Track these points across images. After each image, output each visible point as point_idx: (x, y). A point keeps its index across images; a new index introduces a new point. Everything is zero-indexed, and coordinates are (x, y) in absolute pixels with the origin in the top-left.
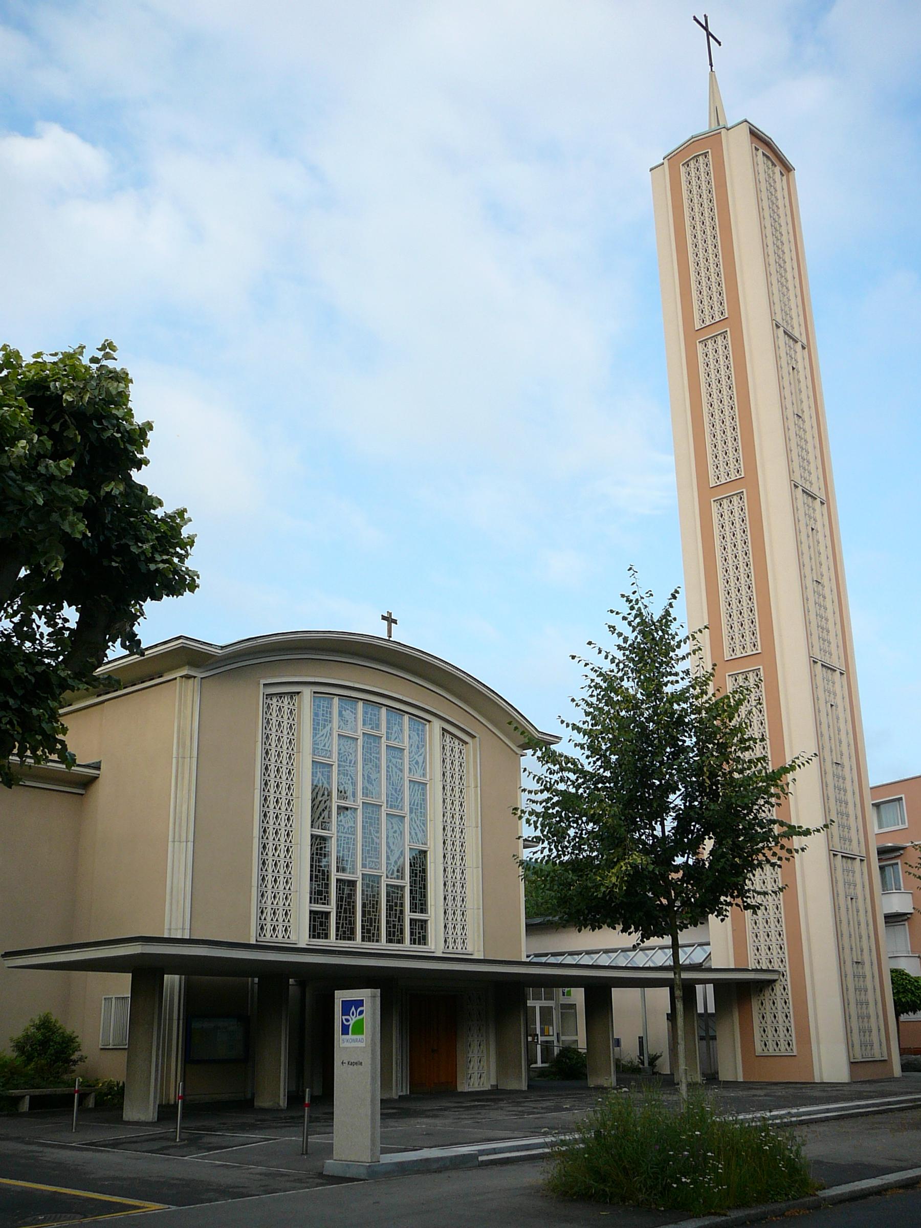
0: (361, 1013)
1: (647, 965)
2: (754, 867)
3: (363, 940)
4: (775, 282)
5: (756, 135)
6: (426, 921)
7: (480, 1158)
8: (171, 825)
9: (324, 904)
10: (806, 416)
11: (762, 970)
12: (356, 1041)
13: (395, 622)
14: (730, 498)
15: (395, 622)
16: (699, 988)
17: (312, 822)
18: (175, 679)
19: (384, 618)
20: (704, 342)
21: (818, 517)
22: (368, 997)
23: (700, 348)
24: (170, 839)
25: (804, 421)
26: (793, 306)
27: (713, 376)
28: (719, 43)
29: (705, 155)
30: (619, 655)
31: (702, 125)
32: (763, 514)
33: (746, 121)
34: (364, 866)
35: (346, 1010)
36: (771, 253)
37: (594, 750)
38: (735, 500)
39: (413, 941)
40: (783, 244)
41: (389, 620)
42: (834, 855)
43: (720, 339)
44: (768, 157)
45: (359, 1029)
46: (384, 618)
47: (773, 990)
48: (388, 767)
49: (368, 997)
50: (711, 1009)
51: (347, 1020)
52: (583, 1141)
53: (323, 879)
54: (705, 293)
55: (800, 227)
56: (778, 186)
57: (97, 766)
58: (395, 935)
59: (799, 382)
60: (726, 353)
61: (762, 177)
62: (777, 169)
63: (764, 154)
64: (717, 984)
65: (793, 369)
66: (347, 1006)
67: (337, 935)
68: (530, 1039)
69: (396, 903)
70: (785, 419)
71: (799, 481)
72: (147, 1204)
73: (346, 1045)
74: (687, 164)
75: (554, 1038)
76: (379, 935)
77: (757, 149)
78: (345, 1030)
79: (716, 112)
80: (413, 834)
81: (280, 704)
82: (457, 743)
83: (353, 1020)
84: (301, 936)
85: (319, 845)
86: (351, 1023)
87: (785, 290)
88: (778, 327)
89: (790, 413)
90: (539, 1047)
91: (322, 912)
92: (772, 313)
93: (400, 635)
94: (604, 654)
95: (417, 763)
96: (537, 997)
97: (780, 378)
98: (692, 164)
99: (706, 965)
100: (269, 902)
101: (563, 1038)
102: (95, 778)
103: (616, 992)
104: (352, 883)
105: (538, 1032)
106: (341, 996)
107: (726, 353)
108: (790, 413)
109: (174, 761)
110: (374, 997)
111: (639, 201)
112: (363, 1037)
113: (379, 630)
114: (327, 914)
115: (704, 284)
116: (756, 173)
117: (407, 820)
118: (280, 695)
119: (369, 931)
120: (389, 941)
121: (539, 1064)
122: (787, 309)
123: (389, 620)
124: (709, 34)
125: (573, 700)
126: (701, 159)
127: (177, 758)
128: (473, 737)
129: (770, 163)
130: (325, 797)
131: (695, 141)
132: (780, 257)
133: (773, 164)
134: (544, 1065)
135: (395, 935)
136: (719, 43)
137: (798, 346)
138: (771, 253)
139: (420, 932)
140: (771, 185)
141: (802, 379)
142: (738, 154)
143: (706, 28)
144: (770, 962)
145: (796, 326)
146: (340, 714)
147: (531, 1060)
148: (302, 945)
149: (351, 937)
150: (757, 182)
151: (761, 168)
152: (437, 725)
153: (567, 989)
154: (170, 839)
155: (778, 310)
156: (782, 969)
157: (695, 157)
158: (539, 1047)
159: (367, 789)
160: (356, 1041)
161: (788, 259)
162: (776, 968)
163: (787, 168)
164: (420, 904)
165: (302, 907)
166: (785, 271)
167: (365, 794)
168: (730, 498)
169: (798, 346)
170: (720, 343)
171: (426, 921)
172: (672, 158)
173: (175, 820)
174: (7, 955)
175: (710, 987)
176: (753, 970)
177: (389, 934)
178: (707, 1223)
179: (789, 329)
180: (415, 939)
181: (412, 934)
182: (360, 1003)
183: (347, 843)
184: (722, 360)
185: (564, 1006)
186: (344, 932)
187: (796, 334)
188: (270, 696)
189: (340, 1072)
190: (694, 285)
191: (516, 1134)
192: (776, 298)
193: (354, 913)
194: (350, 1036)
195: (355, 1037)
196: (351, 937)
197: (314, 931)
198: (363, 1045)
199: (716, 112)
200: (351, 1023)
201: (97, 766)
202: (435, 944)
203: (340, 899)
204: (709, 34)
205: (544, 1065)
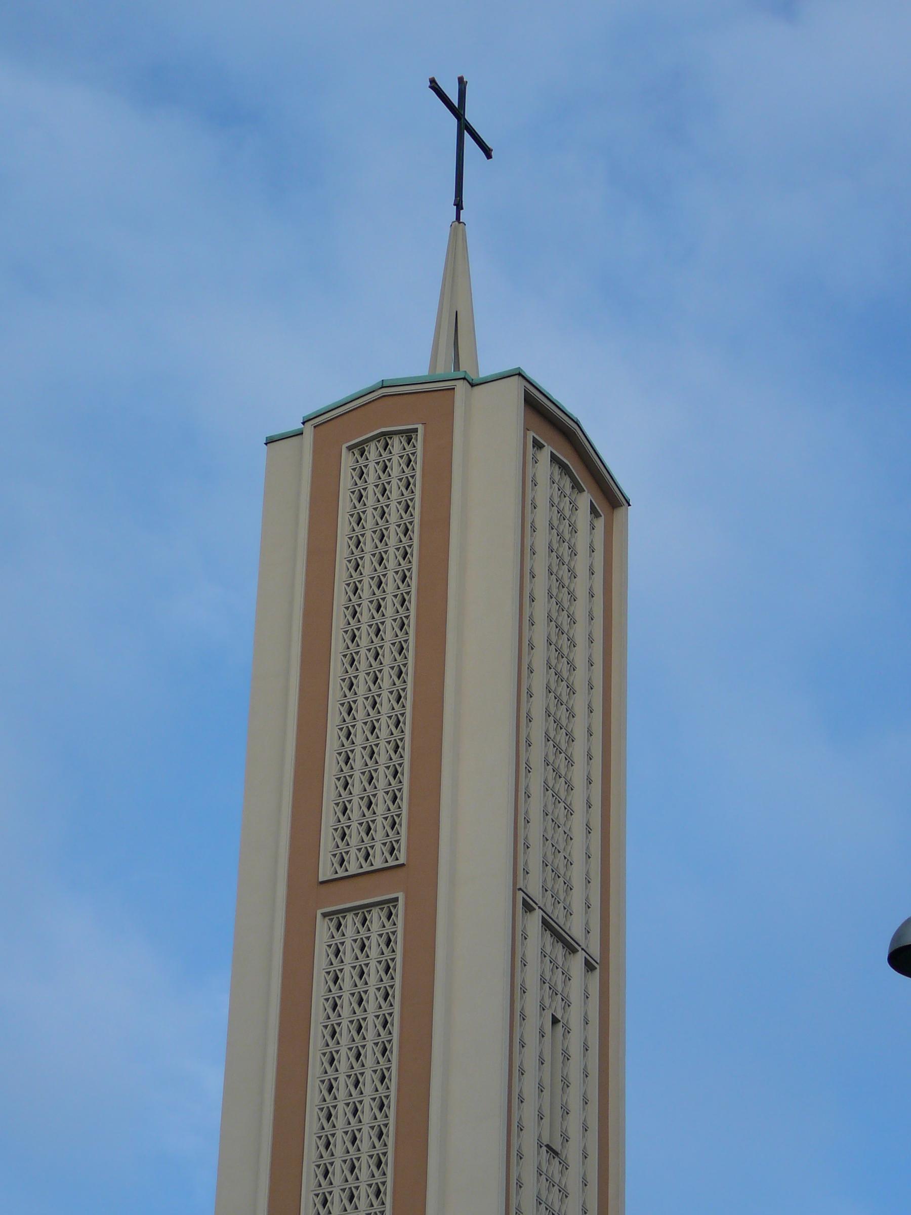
4: (536, 789)
5: (540, 410)
10: (572, 1153)
14: (362, 912)
20: (336, 917)
21: (575, 996)
23: (323, 930)
25: (565, 1166)
26: (578, 856)
27: (348, 958)
28: (488, 153)
29: (409, 435)
31: (410, 357)
32: (433, 1073)
33: (520, 374)
36: (538, 713)
40: (572, 691)
43: (376, 917)
44: (563, 467)
54: (356, 789)
55: (624, 613)
56: (581, 541)
59: (567, 1057)
60: (387, 982)
61: (542, 517)
62: (584, 500)
63: (554, 458)
65: (555, 1021)
70: (512, 1155)
71: (535, 890)
74: (360, 449)
77: (538, 445)
79: (455, 329)
87: (561, 811)
88: (528, 907)
89: (528, 1142)
92: (518, 870)
97: (515, 1043)
98: (373, 451)
107: (387, 982)
108: (528, 1142)
111: (223, 576)
115: (363, 666)
116: (526, 505)
122: (560, 862)
126: (396, 444)
129: (567, 483)
131: (388, 395)
132: (560, 630)
133: (577, 487)
136: (488, 153)
137: (577, 963)
138: (538, 713)
140: (562, 521)
141: (575, 1050)
142: (488, 447)
143: (458, 112)
145: (577, 905)
150: (526, 527)
151: (543, 493)
155: (535, 866)
157: (382, 436)
161: (579, 732)
163: (611, 498)
166: (570, 761)
168: (362, 912)
169: (577, 963)
170: (375, 926)
172: (325, 422)
179: (558, 914)
184: (382, 778)
187: (575, 929)
190: (338, 644)
192: (535, 832)
199: (455, 329)
204: (464, 127)
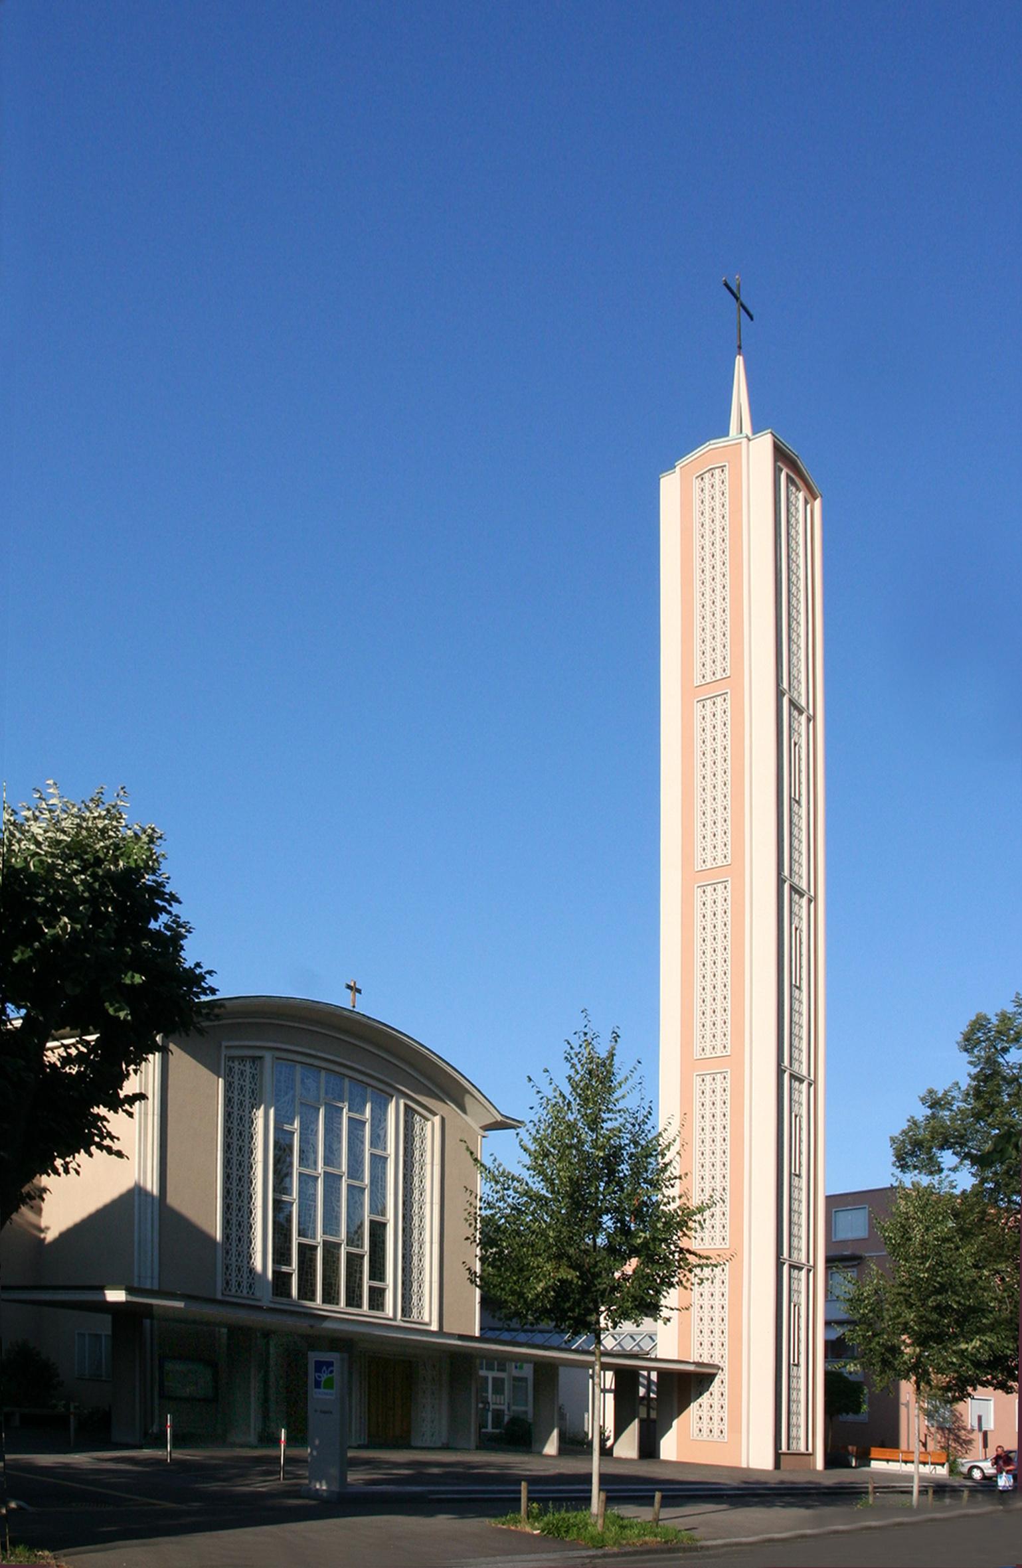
0: (332, 1372)
2: (671, 1285)
15: (359, 991)
29: (722, 468)
30: (533, 1147)
37: (540, 1171)
38: (720, 887)
45: (329, 1384)
46: (349, 987)
58: (354, 1299)
66: (319, 1366)
68: (481, 1406)
75: (505, 1407)
78: (318, 1384)
81: (242, 1067)
86: (323, 1379)
90: (490, 1414)
94: (553, 1086)
100: (234, 1259)
101: (514, 1408)
104: (314, 1248)
106: (314, 1356)
118: (242, 1059)
121: (490, 1429)
125: (467, 1238)
134: (497, 1431)
135: (354, 1299)
146: (302, 1082)
147: (483, 1425)
158: (490, 1414)
162: (716, 1363)
164: (378, 1272)
167: (326, 1164)
176: (694, 1363)
182: (330, 1364)
185: (515, 1379)
188: (231, 1059)
194: (322, 1390)
205: (497, 1431)
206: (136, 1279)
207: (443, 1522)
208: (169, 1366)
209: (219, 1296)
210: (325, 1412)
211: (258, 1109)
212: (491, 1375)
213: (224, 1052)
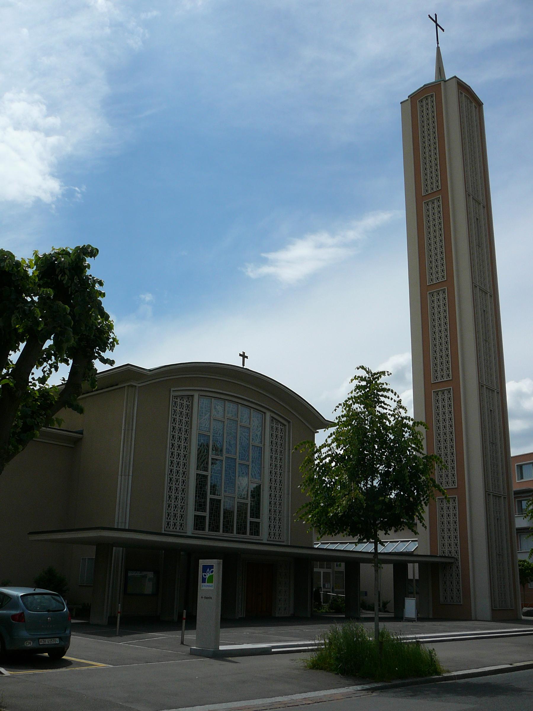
0: (212, 572)
1: (383, 552)
3: (223, 532)
6: (259, 523)
7: (273, 650)
8: (120, 466)
9: (202, 511)
11: (445, 557)
12: (209, 586)
13: (247, 357)
15: (247, 357)
16: (410, 566)
17: (197, 467)
18: (125, 387)
19: (240, 355)
22: (216, 563)
24: (120, 473)
28: (443, 30)
34: (225, 491)
35: (204, 571)
39: (251, 534)
41: (244, 356)
42: (489, 494)
45: (211, 580)
46: (240, 355)
47: (451, 568)
48: (240, 437)
49: (216, 563)
50: (417, 577)
51: (205, 575)
52: (325, 644)
53: (203, 498)
57: (81, 433)
64: (420, 563)
67: (209, 529)
69: (242, 512)
72: (99, 664)
73: (204, 588)
76: (233, 530)
78: (204, 581)
80: (253, 474)
81: (182, 402)
82: (279, 425)
83: (208, 575)
84: (190, 529)
85: (201, 481)
86: (207, 577)
91: (201, 516)
93: (249, 365)
95: (257, 435)
96: (322, 567)
99: (415, 553)
102: (80, 439)
103: (361, 565)
105: (322, 586)
106: (202, 562)
109: (123, 431)
110: (219, 564)
112: (213, 584)
113: (237, 362)
114: (204, 517)
117: (250, 467)
118: (182, 397)
119: (227, 527)
120: (238, 533)
123: (244, 356)
124: (437, 25)
127: (125, 430)
128: (289, 422)
130: (205, 453)
131: (426, 88)
133: (471, 102)
136: (443, 30)
139: (256, 529)
142: (453, 93)
143: (436, 22)
144: (450, 552)
148: (189, 534)
149: (217, 530)
152: (268, 414)
153: (339, 563)
154: (120, 473)
156: (456, 556)
159: (228, 449)
160: (209, 586)
162: (453, 556)
165: (191, 513)
171: (259, 523)
172: (413, 97)
173: (123, 463)
174: (30, 533)
175: (417, 565)
177: (238, 529)
178: (380, 685)
180: (252, 533)
181: (250, 529)
182: (212, 567)
183: (217, 479)
186: (213, 527)
188: (176, 397)
189: (200, 601)
191: (287, 638)
193: (219, 517)
194: (206, 584)
195: (208, 584)
196: (217, 530)
197: (197, 526)
198: (213, 588)
200: (207, 577)
201: (81, 433)
202: (264, 536)
203: (211, 509)
204: (437, 25)
206: (116, 524)
207: (506, 674)
208: (130, 574)
209: (163, 532)
210: (206, 598)
211: (23, 342)
212: (322, 571)
213: (172, 394)
